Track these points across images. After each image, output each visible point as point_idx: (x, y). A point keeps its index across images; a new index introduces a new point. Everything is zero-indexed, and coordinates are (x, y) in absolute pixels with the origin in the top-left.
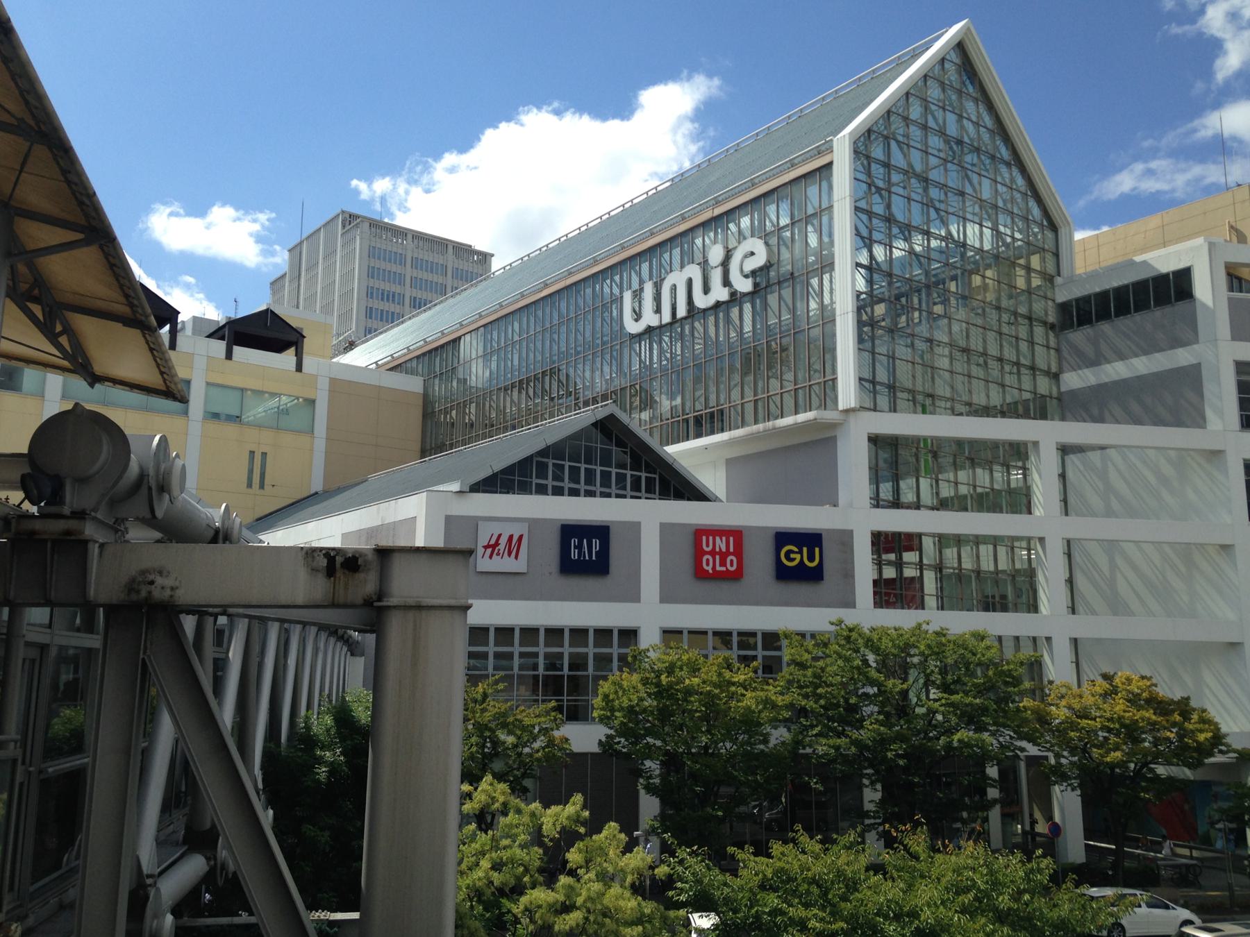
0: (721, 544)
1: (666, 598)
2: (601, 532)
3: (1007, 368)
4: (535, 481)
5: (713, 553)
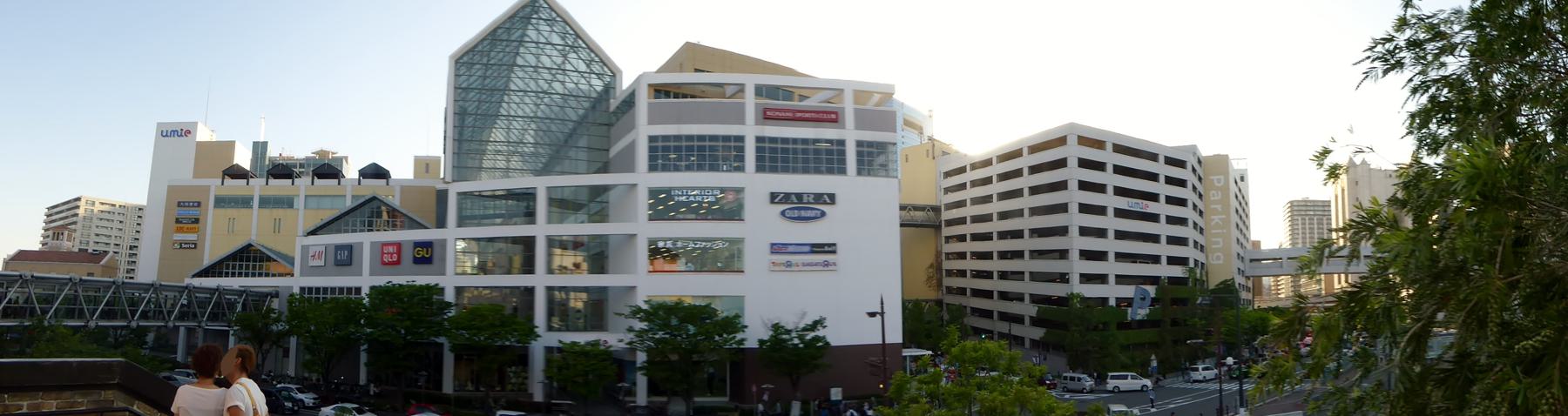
0: (391, 249)
2: (349, 248)
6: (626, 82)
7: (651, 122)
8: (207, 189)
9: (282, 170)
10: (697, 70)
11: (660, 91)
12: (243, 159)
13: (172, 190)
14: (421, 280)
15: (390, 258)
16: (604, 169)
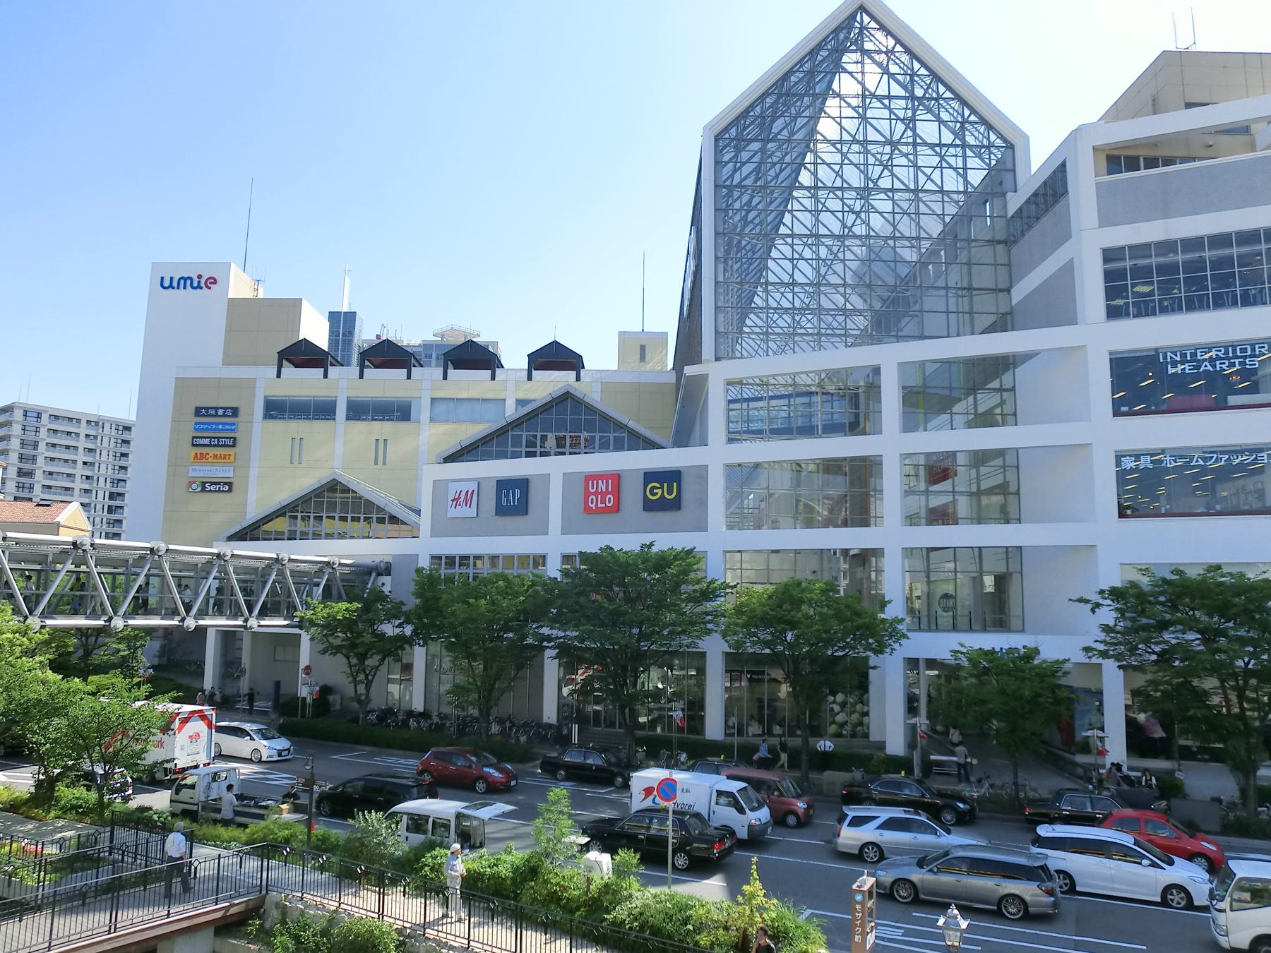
0: (602, 486)
1: (565, 531)
2: (522, 484)
3: (969, 153)
4: (510, 449)
5: (596, 494)
6: (1038, 156)
7: (1106, 220)
8: (251, 384)
9: (387, 355)
10: (1189, 105)
11: (1119, 160)
12: (316, 331)
13: (182, 385)
14: (665, 542)
15: (601, 498)
16: (1002, 324)
